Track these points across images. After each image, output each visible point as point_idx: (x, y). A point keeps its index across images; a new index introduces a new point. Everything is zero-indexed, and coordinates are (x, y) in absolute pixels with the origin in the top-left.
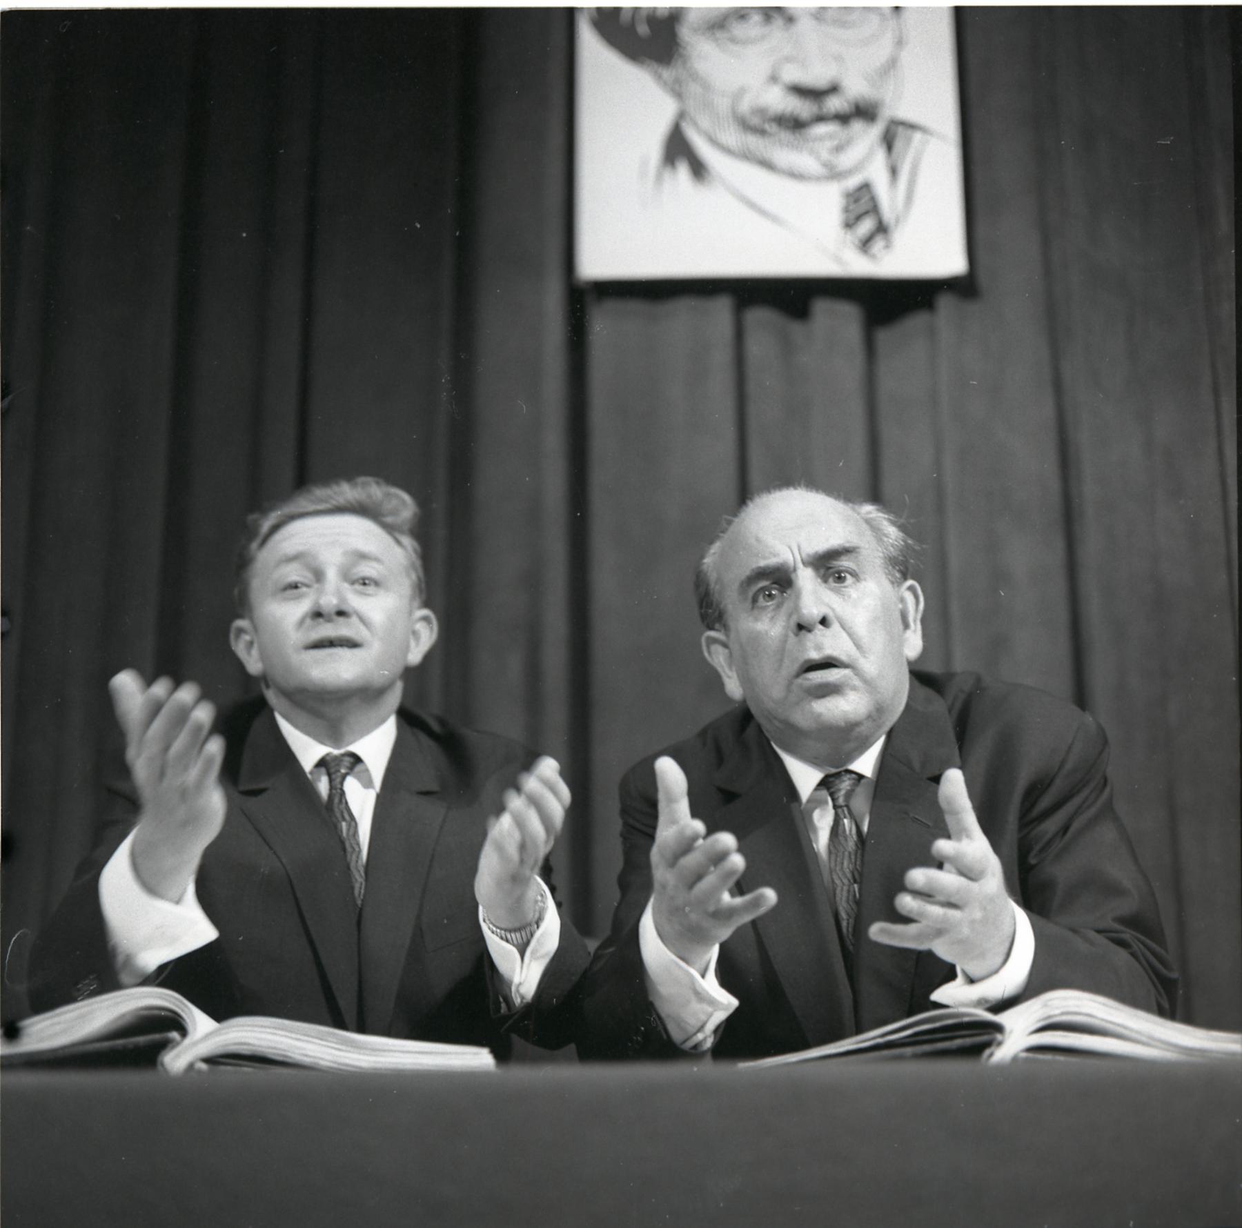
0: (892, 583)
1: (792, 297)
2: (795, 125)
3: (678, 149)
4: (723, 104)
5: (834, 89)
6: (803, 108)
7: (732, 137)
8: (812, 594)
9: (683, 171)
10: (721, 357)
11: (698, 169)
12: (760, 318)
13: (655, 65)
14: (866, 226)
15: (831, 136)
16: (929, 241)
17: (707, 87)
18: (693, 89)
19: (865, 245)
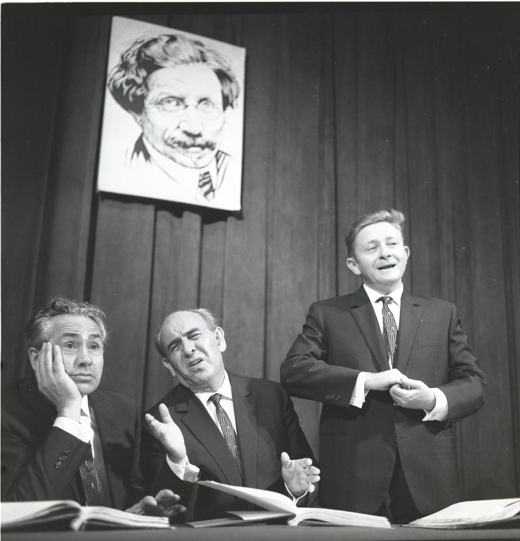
0: (212, 331)
1: (178, 209)
2: (185, 146)
3: (140, 147)
4: (159, 134)
5: (199, 135)
6: (189, 141)
7: (161, 146)
8: (189, 345)
9: (141, 154)
10: (148, 228)
11: (147, 156)
12: (163, 214)
13: (133, 113)
14: (207, 187)
15: (197, 152)
16: (227, 197)
17: (153, 126)
18: (148, 126)
19: (206, 194)
